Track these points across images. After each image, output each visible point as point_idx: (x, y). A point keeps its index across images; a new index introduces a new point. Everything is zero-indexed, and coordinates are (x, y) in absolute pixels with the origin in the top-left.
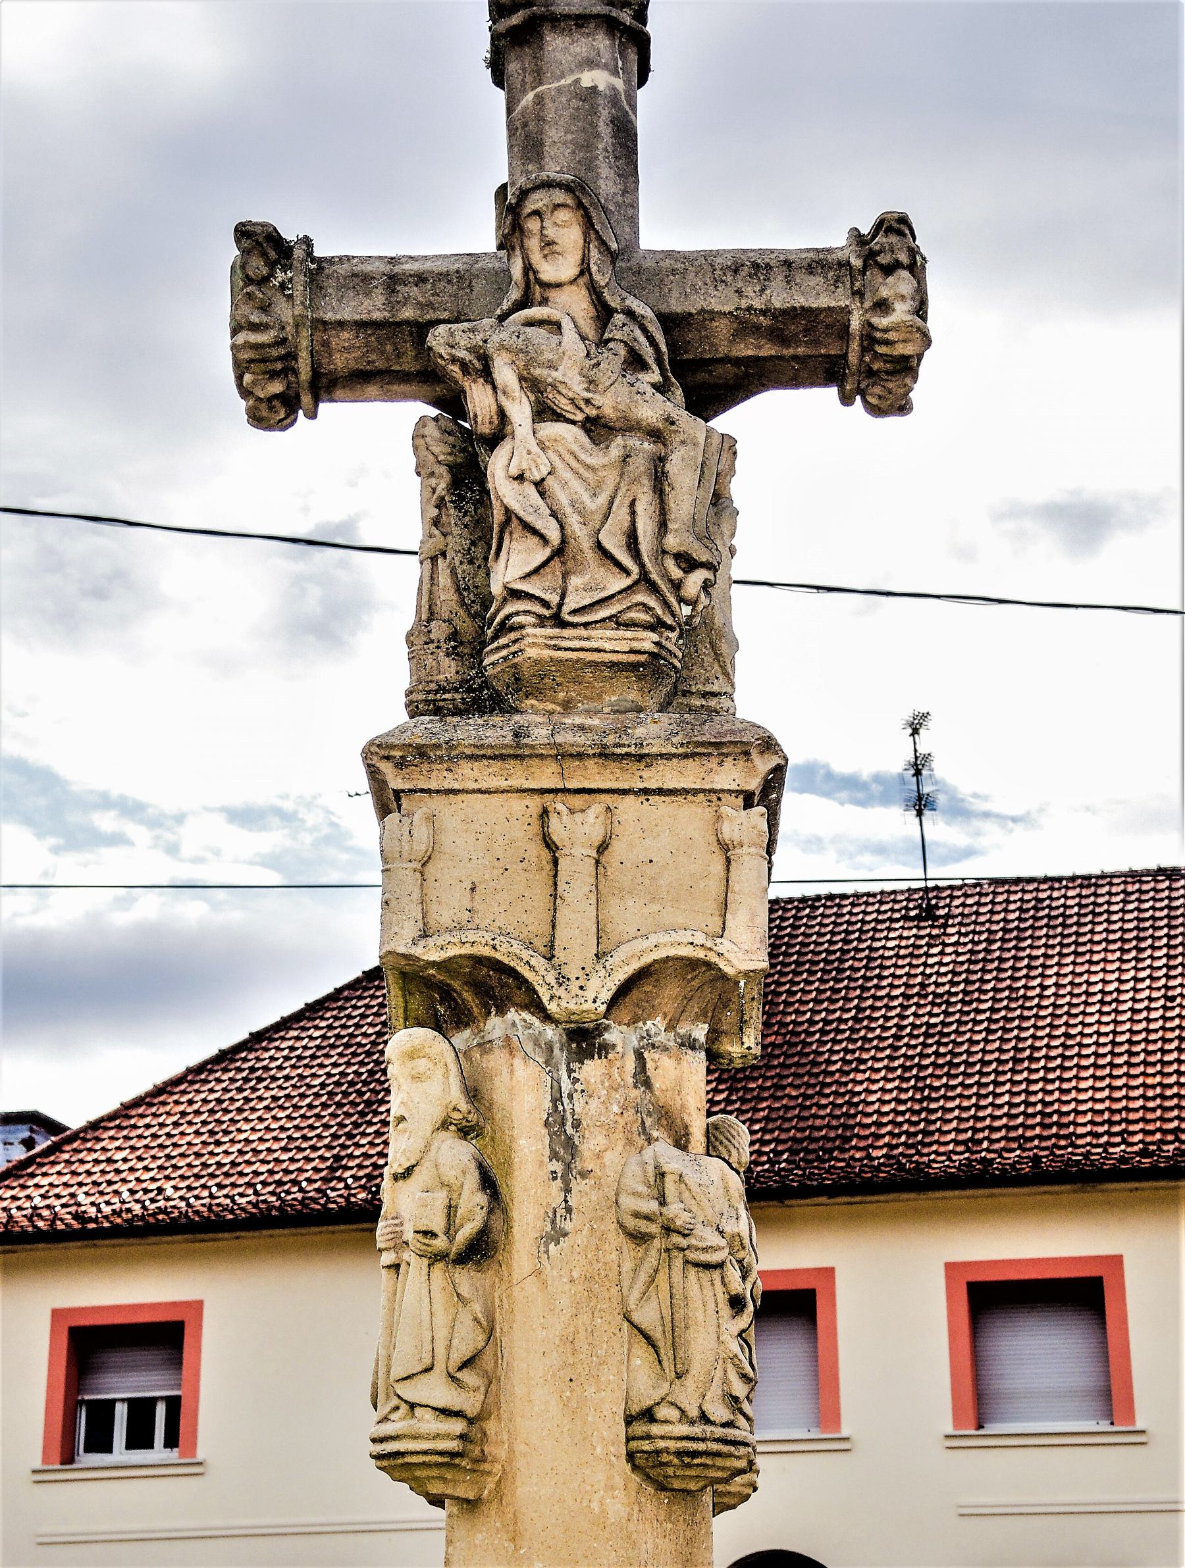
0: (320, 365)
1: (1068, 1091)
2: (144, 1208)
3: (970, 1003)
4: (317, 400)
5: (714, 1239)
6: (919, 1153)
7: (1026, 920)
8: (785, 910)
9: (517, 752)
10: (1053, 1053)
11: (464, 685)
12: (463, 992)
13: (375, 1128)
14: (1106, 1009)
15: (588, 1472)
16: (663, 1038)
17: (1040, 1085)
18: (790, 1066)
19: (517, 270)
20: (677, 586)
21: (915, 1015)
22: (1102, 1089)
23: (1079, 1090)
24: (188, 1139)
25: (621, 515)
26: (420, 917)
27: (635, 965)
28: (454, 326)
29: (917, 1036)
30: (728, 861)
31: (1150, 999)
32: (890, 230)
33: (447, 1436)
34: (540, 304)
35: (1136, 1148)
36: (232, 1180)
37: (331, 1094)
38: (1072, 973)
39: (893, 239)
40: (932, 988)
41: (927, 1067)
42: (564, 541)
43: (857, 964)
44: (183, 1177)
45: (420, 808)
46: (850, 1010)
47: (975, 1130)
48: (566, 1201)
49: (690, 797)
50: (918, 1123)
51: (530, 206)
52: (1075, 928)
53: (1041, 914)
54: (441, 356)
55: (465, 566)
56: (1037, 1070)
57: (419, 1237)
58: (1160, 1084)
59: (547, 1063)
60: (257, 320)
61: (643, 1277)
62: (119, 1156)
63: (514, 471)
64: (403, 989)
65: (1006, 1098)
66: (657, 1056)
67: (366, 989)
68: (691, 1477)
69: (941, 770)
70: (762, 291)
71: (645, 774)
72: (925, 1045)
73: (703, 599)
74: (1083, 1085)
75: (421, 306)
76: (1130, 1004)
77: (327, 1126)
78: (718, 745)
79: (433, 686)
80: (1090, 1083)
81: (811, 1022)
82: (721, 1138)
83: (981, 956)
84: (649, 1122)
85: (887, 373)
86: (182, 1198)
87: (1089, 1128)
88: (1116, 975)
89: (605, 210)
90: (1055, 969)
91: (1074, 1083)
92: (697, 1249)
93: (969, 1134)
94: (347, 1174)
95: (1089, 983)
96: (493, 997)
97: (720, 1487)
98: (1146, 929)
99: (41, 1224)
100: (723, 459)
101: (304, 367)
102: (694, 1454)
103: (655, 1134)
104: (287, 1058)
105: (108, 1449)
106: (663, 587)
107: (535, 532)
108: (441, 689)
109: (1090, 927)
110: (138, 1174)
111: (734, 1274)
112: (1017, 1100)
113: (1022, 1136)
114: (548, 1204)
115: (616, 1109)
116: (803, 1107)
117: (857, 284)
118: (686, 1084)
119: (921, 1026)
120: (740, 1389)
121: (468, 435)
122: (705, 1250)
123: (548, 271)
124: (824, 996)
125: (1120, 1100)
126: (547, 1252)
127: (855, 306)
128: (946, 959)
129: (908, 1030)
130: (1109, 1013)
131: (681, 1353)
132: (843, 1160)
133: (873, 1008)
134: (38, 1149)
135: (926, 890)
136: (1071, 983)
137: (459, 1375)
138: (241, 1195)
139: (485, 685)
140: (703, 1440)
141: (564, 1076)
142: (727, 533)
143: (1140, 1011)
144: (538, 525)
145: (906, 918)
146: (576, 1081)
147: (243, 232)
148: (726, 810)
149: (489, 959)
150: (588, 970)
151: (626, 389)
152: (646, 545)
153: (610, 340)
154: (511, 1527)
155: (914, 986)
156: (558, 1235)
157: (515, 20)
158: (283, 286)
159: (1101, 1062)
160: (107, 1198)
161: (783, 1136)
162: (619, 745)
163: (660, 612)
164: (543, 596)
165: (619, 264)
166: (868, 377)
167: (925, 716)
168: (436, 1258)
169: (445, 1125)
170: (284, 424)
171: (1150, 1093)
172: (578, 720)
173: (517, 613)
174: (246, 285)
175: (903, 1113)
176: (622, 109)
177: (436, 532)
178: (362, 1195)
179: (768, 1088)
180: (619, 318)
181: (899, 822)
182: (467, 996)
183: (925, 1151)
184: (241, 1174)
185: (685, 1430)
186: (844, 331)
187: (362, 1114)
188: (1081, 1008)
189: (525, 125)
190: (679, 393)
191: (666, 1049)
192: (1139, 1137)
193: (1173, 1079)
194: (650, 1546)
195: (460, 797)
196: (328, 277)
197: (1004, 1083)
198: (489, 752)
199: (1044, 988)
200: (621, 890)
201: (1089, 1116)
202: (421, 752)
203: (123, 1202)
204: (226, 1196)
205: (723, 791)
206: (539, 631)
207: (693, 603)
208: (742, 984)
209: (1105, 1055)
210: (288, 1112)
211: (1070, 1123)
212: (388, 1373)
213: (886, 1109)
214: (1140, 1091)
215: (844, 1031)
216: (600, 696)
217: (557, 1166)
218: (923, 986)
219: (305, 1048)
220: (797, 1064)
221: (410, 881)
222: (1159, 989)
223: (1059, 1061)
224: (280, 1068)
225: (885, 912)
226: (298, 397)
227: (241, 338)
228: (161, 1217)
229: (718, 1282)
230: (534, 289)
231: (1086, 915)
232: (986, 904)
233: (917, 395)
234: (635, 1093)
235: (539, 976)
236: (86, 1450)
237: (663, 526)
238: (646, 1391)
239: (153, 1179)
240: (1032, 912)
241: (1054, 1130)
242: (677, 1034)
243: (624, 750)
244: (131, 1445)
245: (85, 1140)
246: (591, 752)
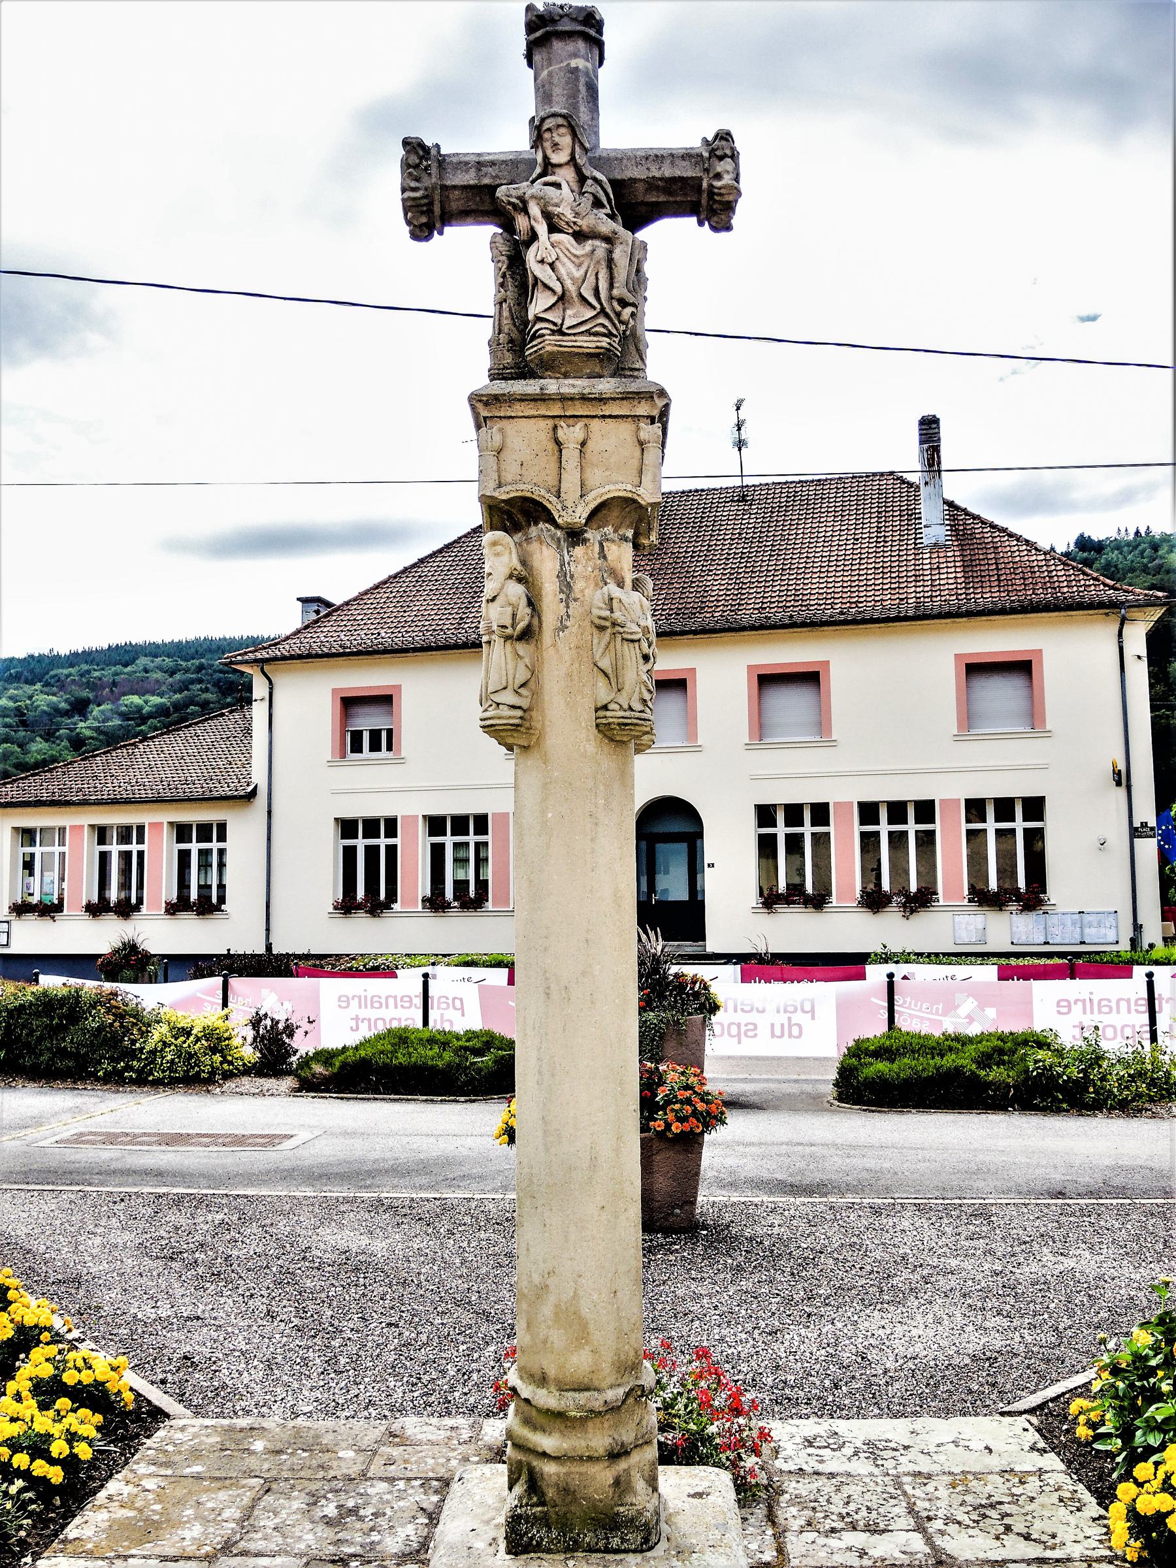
5: (636, 629)
16: (611, 536)
19: (540, 158)
20: (618, 315)
25: (591, 279)
32: (722, 138)
39: (724, 143)
51: (545, 127)
61: (603, 645)
63: (539, 258)
73: (632, 322)
84: (605, 575)
101: (437, 209)
108: (505, 368)
111: (645, 645)
122: (631, 633)
123: (555, 158)
127: (705, 176)
139: (526, 366)
144: (551, 285)
147: (406, 143)
148: (642, 425)
156: (563, 628)
157: (538, 34)
158: (426, 169)
167: (742, 400)
168: (508, 638)
169: (511, 576)
170: (428, 238)
180: (589, 182)
185: (622, 714)
186: (699, 189)
189: (543, 86)
191: (614, 541)
217: (563, 596)
218: (740, 534)
221: (492, 461)
227: (407, 194)
230: (548, 167)
233: (734, 222)
235: (553, 505)
236: (352, 752)
237: (611, 286)
238: (604, 694)
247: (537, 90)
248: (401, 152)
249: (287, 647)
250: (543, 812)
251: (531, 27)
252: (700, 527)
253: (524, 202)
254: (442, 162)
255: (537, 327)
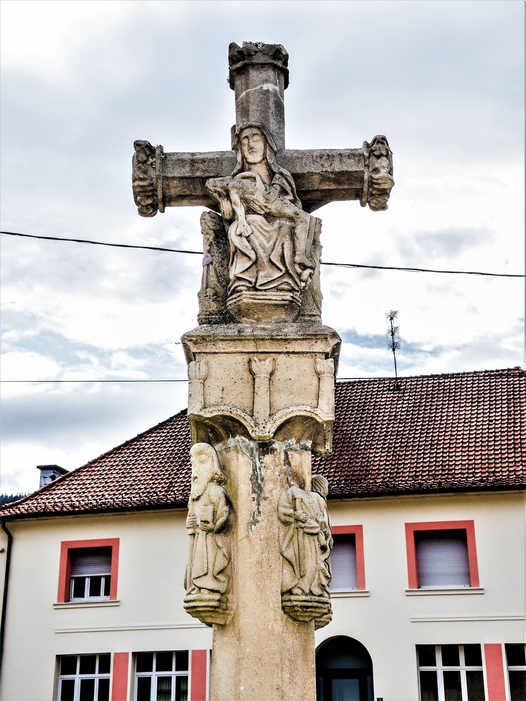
0: (166, 193)
1: (452, 457)
2: (97, 502)
3: (414, 422)
4: (164, 206)
6: (395, 481)
7: (435, 390)
8: (342, 387)
9: (239, 338)
10: (446, 442)
11: (220, 312)
12: (220, 429)
13: (185, 471)
14: (466, 425)
15: (267, 614)
16: (295, 446)
17: (441, 454)
18: (345, 447)
19: (239, 158)
20: (299, 275)
21: (392, 427)
22: (465, 456)
23: (456, 456)
24: (114, 475)
25: (278, 249)
26: (203, 401)
27: (284, 419)
28: (216, 179)
29: (394, 435)
30: (319, 379)
31: (483, 421)
32: (379, 142)
33: (213, 600)
34: (248, 170)
35: (478, 479)
36: (131, 491)
37: (168, 458)
38: (453, 411)
39: (380, 145)
40: (399, 417)
41: (397, 447)
42: (257, 259)
43: (370, 408)
44: (112, 490)
45: (203, 359)
46: (367, 425)
47: (416, 472)
48: (258, 509)
49: (305, 355)
50: (394, 469)
51: (244, 134)
52: (454, 394)
53: (441, 388)
54: (211, 190)
55: (220, 268)
56: (440, 449)
57: (203, 523)
58: (487, 454)
59: (251, 456)
60: (142, 177)
61: (288, 538)
62: (87, 482)
63: (238, 233)
64: (197, 428)
65: (428, 459)
66: (293, 453)
67: (182, 417)
68: (306, 616)
69: (403, 334)
70: (331, 165)
71: (288, 346)
72: (396, 439)
74: (458, 454)
75: (203, 171)
76: (475, 423)
77: (167, 470)
78: (315, 335)
79: (208, 313)
80: (460, 453)
81: (353, 430)
82: (317, 484)
83: (418, 404)
84: (290, 478)
85: (378, 195)
86: (111, 498)
87: (460, 471)
88: (470, 412)
89: (272, 136)
90: (446, 409)
91: (454, 454)
92: (308, 528)
93: (414, 473)
94: (175, 489)
95: (459, 415)
96: (230, 431)
97: (318, 620)
98: (481, 394)
99: (57, 509)
100: (317, 227)
102: (308, 607)
103: (292, 483)
104: (152, 444)
105: (83, 596)
106: (294, 276)
107: (246, 256)
109: (459, 393)
110: (94, 489)
111: (322, 537)
112: (432, 460)
113: (434, 474)
114: (251, 510)
115: (277, 473)
116: (350, 463)
117: (367, 162)
118: (303, 463)
119: (395, 431)
120: (325, 582)
121: (221, 219)
122: (311, 528)
123: (251, 159)
124: (357, 420)
125: (472, 460)
126: (251, 529)
128: (405, 406)
129: (390, 433)
130: (467, 427)
131: (302, 568)
132: (366, 483)
133: (376, 424)
134: (57, 480)
135: (396, 379)
136: (452, 415)
137: (218, 577)
138: (134, 497)
139: (228, 312)
140: (311, 602)
141: (258, 461)
142: (318, 255)
143: (479, 426)
144: (247, 253)
145: (389, 390)
146: (262, 463)
147: (137, 144)
148: (318, 360)
149: (229, 416)
150: (266, 421)
151: (280, 202)
152: (288, 260)
153: (274, 184)
154: (238, 635)
155: (392, 416)
156: (255, 522)
157: (239, 65)
158: (152, 164)
159: (464, 445)
160: (83, 498)
161: (342, 474)
162: (278, 335)
163: (293, 285)
164: (249, 279)
165: (277, 155)
166: (371, 196)
167: (395, 313)
169: (212, 480)
170: (152, 215)
171: (484, 458)
172: (262, 326)
173: (239, 286)
174: (138, 164)
175: (388, 465)
176: (278, 98)
177: (209, 255)
178: (181, 497)
179: (337, 455)
180: (277, 176)
181: (386, 354)
182: (221, 430)
183: (397, 480)
184: (134, 489)
185: (304, 598)
186: (362, 178)
187: (181, 466)
188: (457, 424)
189: (242, 104)
190: (300, 203)
191: (296, 450)
192: (480, 474)
193: (492, 452)
194: (291, 642)
195: (219, 355)
196: (169, 160)
197: (427, 454)
198: (229, 338)
199: (442, 417)
200: (279, 390)
201: (460, 467)
202: (203, 338)
203: (89, 500)
204: (128, 498)
205: (317, 352)
206: (247, 292)
207: (306, 282)
208: (325, 425)
209: (466, 443)
210: (152, 465)
211: (453, 469)
212: (191, 576)
213: (382, 463)
214: (480, 457)
215: (365, 433)
216: (271, 317)
217: (255, 496)
218: (396, 416)
219: (159, 440)
220: (348, 446)
221: (200, 387)
222: (486, 417)
223: (448, 445)
224: (149, 448)
225: (381, 387)
226: (157, 205)
227: (136, 183)
228: (103, 506)
229: (316, 540)
230: (245, 166)
231: (458, 389)
232: (419, 385)
234: (284, 468)
235: (248, 422)
237: (294, 253)
238: (289, 582)
239: (100, 491)
240: (437, 388)
241: (447, 472)
242: (300, 445)
243: (279, 337)
244: (92, 594)
245: (74, 476)
246: (267, 338)
247: (237, 106)
248: (132, 151)
249: (26, 507)
250: (237, 685)
251: (232, 60)
252: (364, 410)
253: (227, 191)
254: (165, 158)
255: (236, 284)
